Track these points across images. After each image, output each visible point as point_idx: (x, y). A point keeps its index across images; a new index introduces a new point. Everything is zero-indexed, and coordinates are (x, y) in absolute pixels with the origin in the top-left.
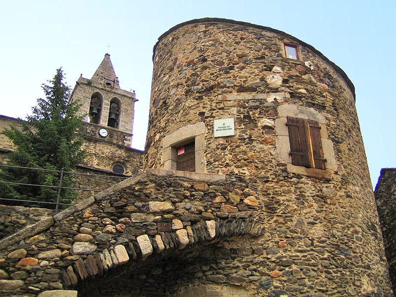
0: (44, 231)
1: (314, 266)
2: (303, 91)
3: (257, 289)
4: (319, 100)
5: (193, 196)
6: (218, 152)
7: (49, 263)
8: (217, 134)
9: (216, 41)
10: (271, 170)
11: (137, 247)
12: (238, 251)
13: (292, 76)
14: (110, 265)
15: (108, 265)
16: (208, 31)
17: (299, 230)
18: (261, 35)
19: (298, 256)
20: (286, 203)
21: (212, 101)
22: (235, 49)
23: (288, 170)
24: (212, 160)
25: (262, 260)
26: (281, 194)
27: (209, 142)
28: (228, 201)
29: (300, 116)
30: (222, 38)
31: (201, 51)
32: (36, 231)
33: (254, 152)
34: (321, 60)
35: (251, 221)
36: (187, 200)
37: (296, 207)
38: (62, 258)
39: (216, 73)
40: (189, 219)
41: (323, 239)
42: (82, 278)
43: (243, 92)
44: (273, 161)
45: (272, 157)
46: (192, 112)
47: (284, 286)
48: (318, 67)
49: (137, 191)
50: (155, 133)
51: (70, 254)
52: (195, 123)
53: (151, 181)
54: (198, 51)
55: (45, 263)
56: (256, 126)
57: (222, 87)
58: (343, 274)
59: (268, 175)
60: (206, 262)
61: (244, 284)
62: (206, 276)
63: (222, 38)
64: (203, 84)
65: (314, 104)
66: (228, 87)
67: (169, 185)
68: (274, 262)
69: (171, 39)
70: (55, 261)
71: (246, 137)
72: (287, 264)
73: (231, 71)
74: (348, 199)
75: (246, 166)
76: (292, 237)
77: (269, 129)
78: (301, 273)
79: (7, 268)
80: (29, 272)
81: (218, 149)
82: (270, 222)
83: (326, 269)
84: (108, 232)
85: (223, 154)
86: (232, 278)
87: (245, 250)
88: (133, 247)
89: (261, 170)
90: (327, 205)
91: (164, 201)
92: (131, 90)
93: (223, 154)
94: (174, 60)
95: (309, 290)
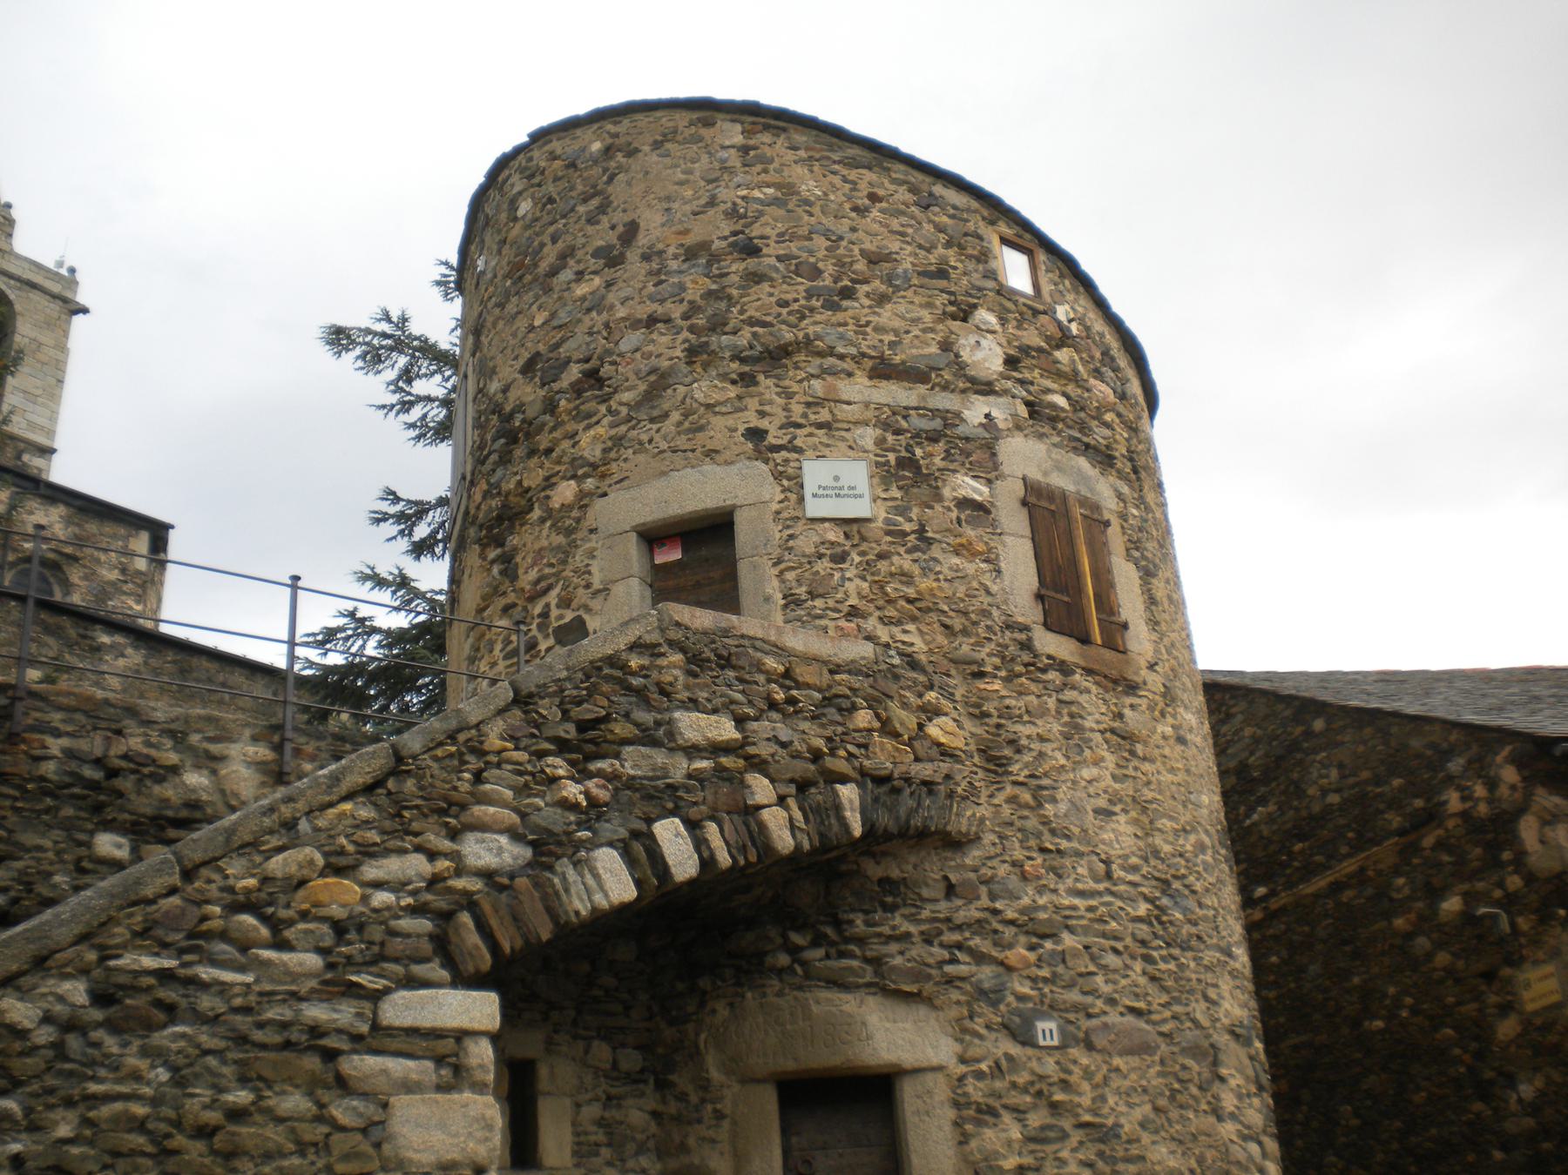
0: (369, 789)
1: (1116, 938)
2: (1061, 401)
3: (968, 1003)
4: (1099, 435)
5: (792, 701)
6: (823, 566)
7: (398, 898)
8: (814, 508)
9: (788, 189)
10: (989, 639)
12: (902, 889)
13: (1029, 347)
14: (584, 913)
15: (577, 913)
16: (755, 148)
17: (1076, 830)
18: (931, 194)
19: (1074, 908)
20: (1036, 746)
21: (789, 396)
23: (1037, 644)
24: (801, 591)
25: (978, 915)
26: (1020, 716)
27: (790, 532)
29: (1059, 481)
31: (733, 213)
32: (345, 786)
33: (938, 580)
34: (1090, 305)
35: (951, 795)
36: (775, 715)
37: (1063, 761)
38: (434, 881)
39: (796, 300)
40: (788, 776)
41: (1134, 860)
42: (507, 949)
43: (887, 377)
44: (995, 613)
45: (989, 599)
46: (719, 422)
47: (1043, 995)
48: (1088, 329)
49: (634, 674)
50: (547, 479)
51: (459, 872)
52: (732, 463)
53: (671, 643)
54: (726, 213)
55: (382, 898)
56: (939, 498)
57: (820, 354)
58: (1181, 966)
59: (983, 655)
60: (792, 919)
61: (929, 988)
62: (804, 964)
63: (810, 186)
64: (755, 335)
65: (1087, 446)
66: (842, 357)
67: (725, 662)
68: (1012, 922)
69: (596, 146)
70: (414, 893)
71: (908, 527)
72: (1047, 931)
73: (845, 303)
74: (1179, 748)
75: (914, 619)
76: (1059, 851)
77: (978, 510)
78: (1087, 958)
79: (270, 910)
80: (339, 928)
81: (821, 556)
82: (996, 801)
83: (1144, 951)
85: (837, 575)
86: (893, 968)
87: (927, 885)
88: (642, 853)
89: (960, 639)
90: (1135, 763)
91: (715, 711)
92: (60, 264)
93: (837, 575)
94: (620, 229)
95: (1107, 1008)
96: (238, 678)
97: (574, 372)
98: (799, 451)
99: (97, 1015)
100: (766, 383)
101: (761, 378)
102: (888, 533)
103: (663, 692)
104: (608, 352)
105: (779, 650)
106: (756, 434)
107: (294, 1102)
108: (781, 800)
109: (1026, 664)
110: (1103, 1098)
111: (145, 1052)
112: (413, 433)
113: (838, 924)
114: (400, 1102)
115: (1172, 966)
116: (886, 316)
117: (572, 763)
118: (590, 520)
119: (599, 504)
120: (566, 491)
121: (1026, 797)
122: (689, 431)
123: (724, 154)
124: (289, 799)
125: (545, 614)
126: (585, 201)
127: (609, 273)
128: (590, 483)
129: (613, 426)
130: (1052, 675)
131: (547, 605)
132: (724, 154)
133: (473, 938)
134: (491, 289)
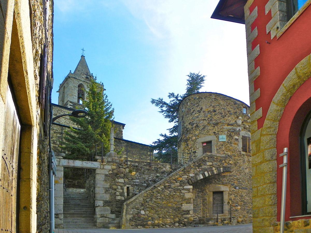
2: (248, 126)
5: (217, 160)
8: (220, 140)
9: (220, 104)
11: (205, 175)
20: (240, 163)
22: (227, 108)
23: (241, 153)
28: (225, 162)
30: (222, 102)
31: (213, 107)
32: (181, 171)
44: (237, 150)
51: (189, 177)
55: (184, 179)
56: (233, 138)
67: (211, 157)
69: (198, 97)
71: (229, 142)
73: (225, 117)
80: (181, 181)
81: (220, 145)
84: (198, 171)
88: (204, 175)
91: (210, 162)
92: (101, 82)
94: (200, 108)
96: (138, 145)
97: (195, 125)
98: (219, 134)
99: (164, 188)
100: (216, 127)
101: (215, 126)
102: (227, 143)
103: (206, 161)
104: (199, 123)
105: (217, 156)
106: (214, 133)
107: (178, 194)
108: (215, 170)
109: (240, 155)
110: (242, 193)
111: (168, 191)
112: (165, 117)
113: (219, 179)
114: (185, 194)
115: (250, 182)
116: (230, 118)
117: (198, 167)
118: (197, 141)
119: (198, 139)
120: (194, 138)
121: (238, 168)
122: (207, 132)
123: (212, 99)
124: (177, 172)
125: (192, 150)
126: (196, 104)
127: (199, 114)
128: (197, 137)
129: (199, 131)
130: (243, 156)
131: (192, 150)
132: (212, 99)
133: (190, 182)
134: (184, 113)
